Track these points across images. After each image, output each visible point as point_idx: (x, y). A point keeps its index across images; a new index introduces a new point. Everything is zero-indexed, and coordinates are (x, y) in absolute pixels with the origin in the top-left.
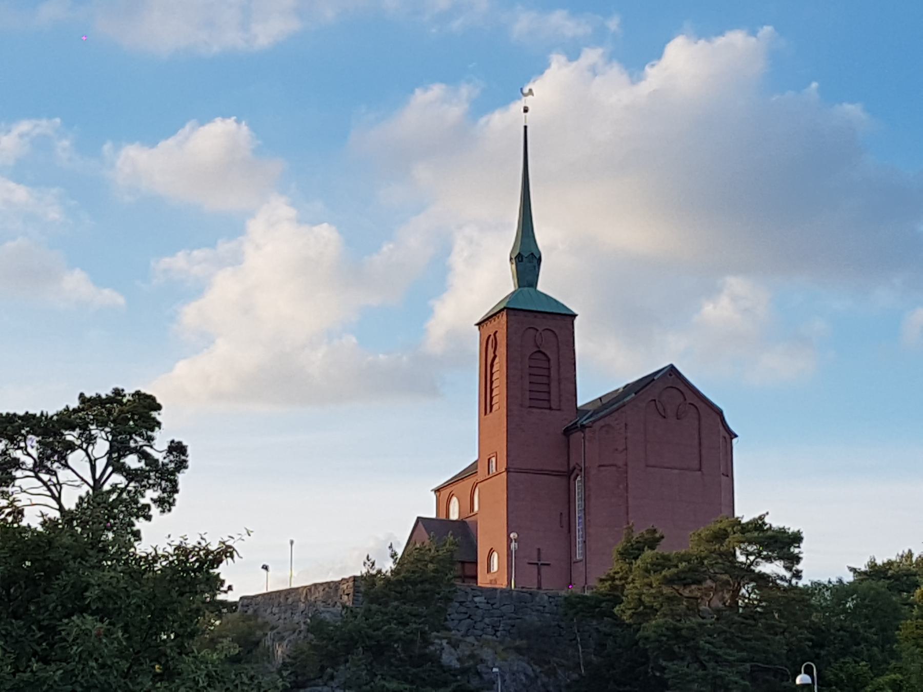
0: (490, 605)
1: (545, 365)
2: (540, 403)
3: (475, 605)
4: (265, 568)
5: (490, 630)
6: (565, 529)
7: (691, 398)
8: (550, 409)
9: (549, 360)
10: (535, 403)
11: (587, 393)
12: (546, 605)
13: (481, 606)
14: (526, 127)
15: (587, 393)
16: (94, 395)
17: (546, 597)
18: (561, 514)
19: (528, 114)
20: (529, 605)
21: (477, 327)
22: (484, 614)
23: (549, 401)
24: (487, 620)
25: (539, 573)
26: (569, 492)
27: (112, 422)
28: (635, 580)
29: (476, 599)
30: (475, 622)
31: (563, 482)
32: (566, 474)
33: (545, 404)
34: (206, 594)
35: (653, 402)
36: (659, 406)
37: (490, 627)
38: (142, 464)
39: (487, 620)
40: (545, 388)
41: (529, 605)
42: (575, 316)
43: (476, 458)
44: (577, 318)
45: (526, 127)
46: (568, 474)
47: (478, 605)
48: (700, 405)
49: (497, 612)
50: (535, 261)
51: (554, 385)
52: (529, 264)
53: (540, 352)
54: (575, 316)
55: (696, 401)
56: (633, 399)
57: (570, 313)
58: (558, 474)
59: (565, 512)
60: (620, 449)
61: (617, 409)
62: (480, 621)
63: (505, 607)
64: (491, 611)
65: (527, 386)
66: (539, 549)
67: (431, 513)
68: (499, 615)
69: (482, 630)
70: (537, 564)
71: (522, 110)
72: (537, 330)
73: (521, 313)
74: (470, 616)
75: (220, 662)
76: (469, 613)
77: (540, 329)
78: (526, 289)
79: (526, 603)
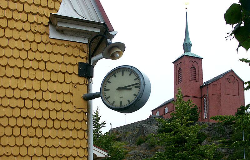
2: (193, 80)
4: (111, 124)
7: (236, 78)
9: (195, 69)
10: (192, 80)
26: (202, 102)
31: (200, 99)
33: (195, 80)
35: (227, 79)
36: (229, 79)
40: (195, 76)
46: (202, 98)
48: (238, 80)
50: (191, 45)
51: (197, 76)
52: (189, 46)
53: (193, 67)
55: (238, 80)
56: (222, 77)
58: (199, 98)
59: (201, 107)
60: (219, 90)
65: (190, 72)
67: (92, 78)
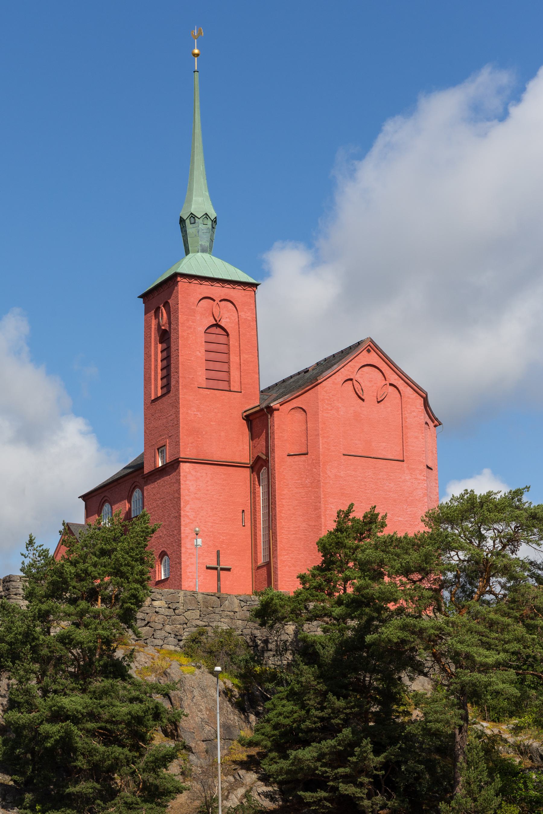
0: (172, 610)
1: (222, 339)
3: (154, 610)
5: (171, 639)
11: (145, 473)
12: (237, 610)
13: (162, 611)
15: (145, 473)
17: (236, 601)
18: (243, 511)
20: (217, 610)
21: (141, 300)
22: (164, 621)
24: (168, 628)
25: (219, 579)
29: (156, 603)
30: (155, 631)
32: (249, 466)
33: (223, 385)
35: (299, 415)
36: (357, 385)
37: (173, 635)
39: (168, 628)
41: (217, 610)
43: (142, 450)
47: (157, 610)
49: (181, 619)
61: (343, 367)
62: (161, 629)
63: (189, 612)
64: (173, 617)
68: (182, 622)
69: (163, 640)
70: (216, 569)
72: (214, 300)
74: (148, 623)
75: (262, 662)
76: (147, 619)
78: (199, 254)
79: (213, 608)
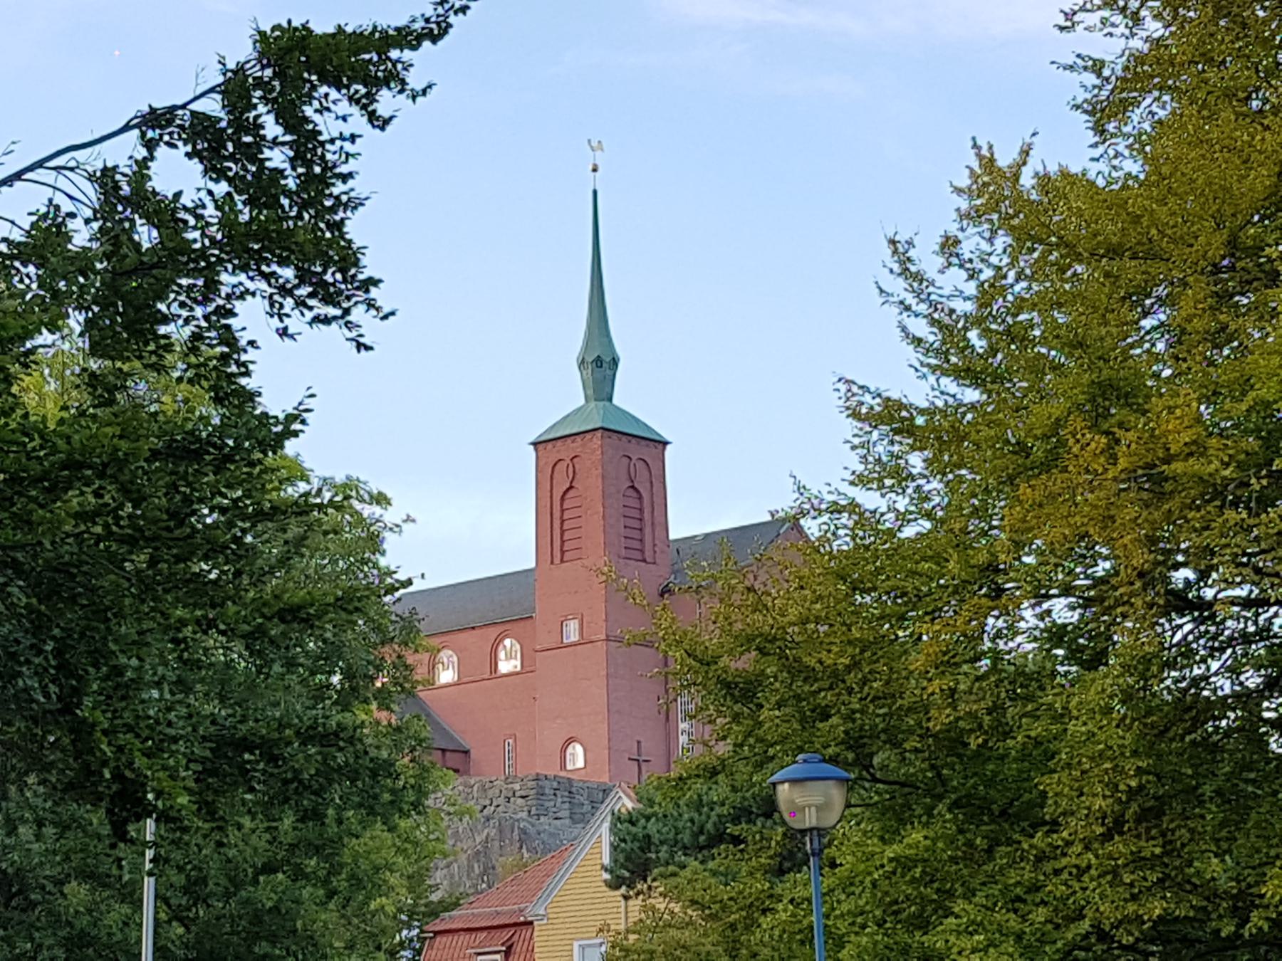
1: (635, 504)
6: (663, 716)
8: (644, 561)
9: (640, 498)
14: (595, 193)
16: (331, 30)
19: (597, 174)
21: (532, 447)
23: (642, 551)
27: (57, 740)
28: (371, 497)
33: (638, 555)
34: (264, 944)
38: (179, 281)
42: (665, 443)
44: (668, 447)
45: (595, 193)
51: (648, 530)
54: (665, 443)
57: (657, 438)
66: (639, 742)
71: (591, 167)
73: (615, 436)
77: (634, 458)
